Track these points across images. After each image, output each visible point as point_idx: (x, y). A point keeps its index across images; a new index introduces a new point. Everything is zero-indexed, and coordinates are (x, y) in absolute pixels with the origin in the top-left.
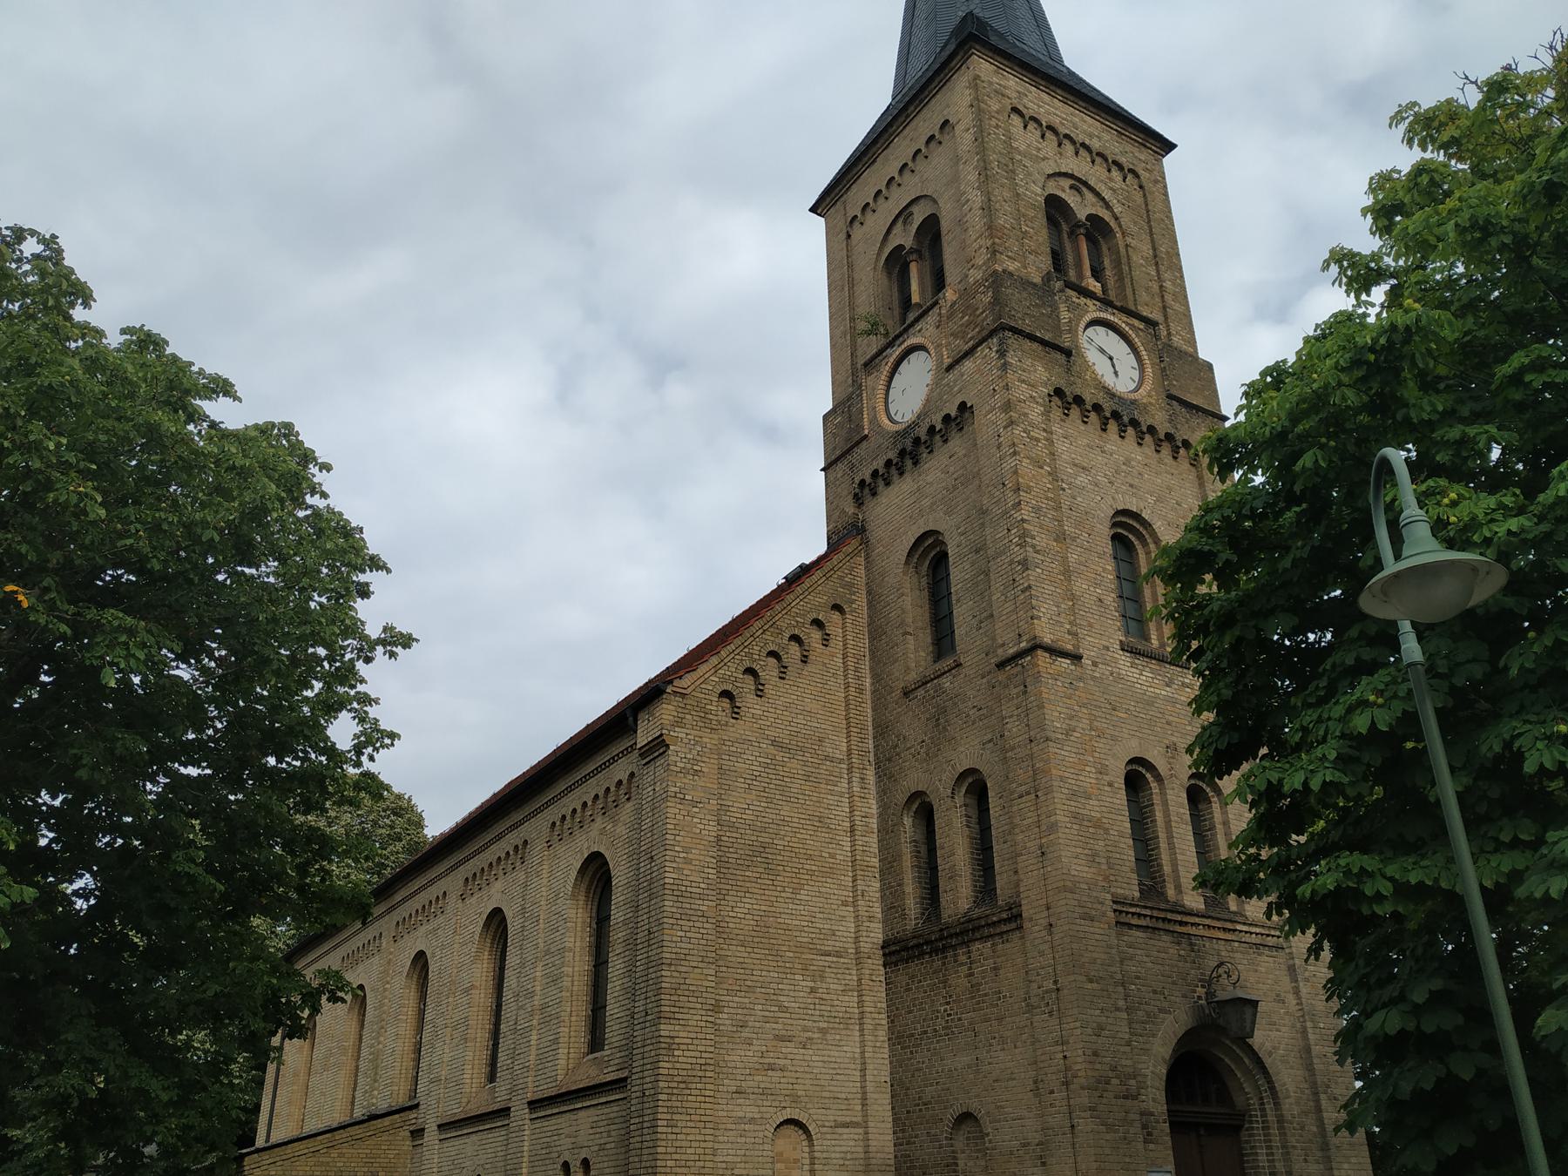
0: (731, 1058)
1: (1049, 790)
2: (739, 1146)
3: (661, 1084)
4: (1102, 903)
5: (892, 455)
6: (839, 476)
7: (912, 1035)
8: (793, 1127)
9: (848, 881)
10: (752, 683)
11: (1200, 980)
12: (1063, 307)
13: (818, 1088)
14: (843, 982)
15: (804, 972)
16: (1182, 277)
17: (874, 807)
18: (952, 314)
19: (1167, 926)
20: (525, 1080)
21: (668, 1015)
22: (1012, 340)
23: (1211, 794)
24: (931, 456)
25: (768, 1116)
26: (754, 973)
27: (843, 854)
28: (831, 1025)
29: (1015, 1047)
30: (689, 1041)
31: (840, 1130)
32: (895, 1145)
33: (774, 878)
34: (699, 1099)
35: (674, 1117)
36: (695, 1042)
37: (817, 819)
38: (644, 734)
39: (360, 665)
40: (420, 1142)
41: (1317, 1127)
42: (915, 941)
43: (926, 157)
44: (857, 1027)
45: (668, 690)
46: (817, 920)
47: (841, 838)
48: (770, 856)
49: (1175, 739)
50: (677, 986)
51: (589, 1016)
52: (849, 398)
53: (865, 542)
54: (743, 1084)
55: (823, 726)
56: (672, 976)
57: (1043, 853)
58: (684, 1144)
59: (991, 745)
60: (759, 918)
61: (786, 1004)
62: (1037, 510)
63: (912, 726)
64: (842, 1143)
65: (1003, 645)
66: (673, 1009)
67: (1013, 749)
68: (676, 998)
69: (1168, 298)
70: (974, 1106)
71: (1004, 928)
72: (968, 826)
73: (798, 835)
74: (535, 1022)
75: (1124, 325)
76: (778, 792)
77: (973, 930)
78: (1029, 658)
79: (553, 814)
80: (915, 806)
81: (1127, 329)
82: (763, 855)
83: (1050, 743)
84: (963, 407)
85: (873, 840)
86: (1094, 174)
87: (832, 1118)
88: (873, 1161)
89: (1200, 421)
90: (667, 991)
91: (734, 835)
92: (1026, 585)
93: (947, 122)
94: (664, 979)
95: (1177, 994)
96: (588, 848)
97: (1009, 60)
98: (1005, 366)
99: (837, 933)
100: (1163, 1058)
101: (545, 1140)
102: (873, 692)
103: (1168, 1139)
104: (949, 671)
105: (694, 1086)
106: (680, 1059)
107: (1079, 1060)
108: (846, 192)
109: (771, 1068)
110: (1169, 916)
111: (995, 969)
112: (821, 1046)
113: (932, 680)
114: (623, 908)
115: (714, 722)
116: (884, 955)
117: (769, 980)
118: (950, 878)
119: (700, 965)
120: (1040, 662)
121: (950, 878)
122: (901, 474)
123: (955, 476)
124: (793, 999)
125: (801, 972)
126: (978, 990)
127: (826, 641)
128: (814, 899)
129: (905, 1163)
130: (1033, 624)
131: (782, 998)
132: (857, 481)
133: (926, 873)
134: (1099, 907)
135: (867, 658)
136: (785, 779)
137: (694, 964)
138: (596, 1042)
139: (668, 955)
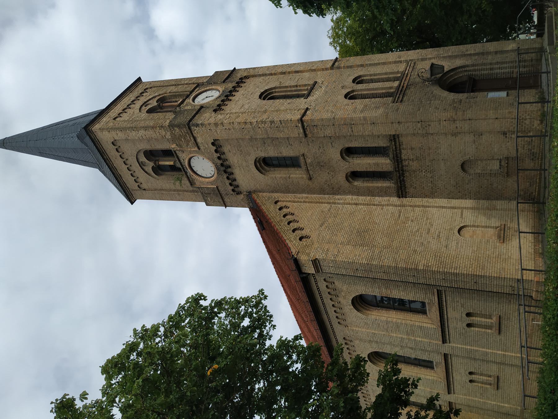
0: (434, 248)
1: (352, 119)
2: (466, 248)
3: (441, 270)
4: (393, 106)
5: (225, 176)
6: (229, 201)
7: (432, 187)
8: (461, 232)
9: (374, 207)
10: (298, 231)
11: (423, 83)
12: (186, 108)
13: (448, 222)
14: (410, 211)
15: (405, 223)
16: (184, 79)
17: (349, 197)
18: (180, 146)
19: (403, 91)
20: (434, 344)
21: (416, 266)
22: (194, 121)
23: (360, 79)
24: (228, 160)
25: (456, 238)
26: (403, 238)
27: (365, 208)
28: (426, 216)
29: (440, 143)
30: (426, 260)
31: (464, 217)
32: (470, 199)
33: (370, 230)
34: (448, 258)
35: (453, 267)
36: (426, 258)
37: (350, 215)
38: (310, 269)
39: (268, 339)
40: (454, 404)
41: (476, 56)
42: (399, 183)
43: (123, 153)
44: (427, 208)
45: (296, 257)
46: (387, 218)
47: (359, 208)
48: (362, 230)
49: (340, 86)
50: (405, 263)
51: (413, 314)
52: (202, 193)
53: (255, 192)
54: (444, 245)
55: (318, 210)
56: (401, 264)
57: (373, 123)
58: (464, 264)
59: (333, 143)
60: (384, 236)
61: (416, 230)
62: (254, 117)
63: (322, 177)
64: (468, 216)
65: (299, 134)
66: (414, 264)
67: (335, 133)
68: (410, 263)
69: (190, 82)
70: (459, 163)
71: (398, 144)
72: (361, 157)
73: (356, 221)
74: (413, 338)
75: (196, 93)
76: (339, 226)
77: (397, 157)
78: (305, 123)
79: (335, 322)
80: (351, 180)
81: (198, 92)
82: (361, 232)
83: (336, 117)
84: (213, 144)
85: (360, 198)
86: (143, 100)
87: (459, 219)
88: (476, 206)
89: (234, 75)
90: (407, 266)
91: (352, 241)
92: (279, 122)
93: (113, 143)
94: (402, 266)
95: (427, 89)
96: (350, 305)
97: (96, 119)
98: (202, 124)
99: (393, 212)
100: (448, 93)
101: (458, 336)
102: (308, 194)
103: (476, 93)
104: (305, 159)
105: (443, 260)
106: (432, 263)
107: (446, 114)
108: (129, 189)
109: (439, 236)
110: (400, 90)
111: (411, 149)
112: (433, 220)
113: (307, 167)
114: (374, 289)
115: (310, 243)
116: (402, 197)
117: (406, 234)
118: (378, 166)
119: (398, 254)
120: (307, 119)
121: (378, 166)
122: (233, 174)
123: (237, 150)
124: (415, 227)
125: (405, 224)
126: (419, 157)
127: (287, 207)
128: (379, 218)
129: (477, 195)
130: (293, 120)
131: (414, 231)
132: (232, 193)
133: (375, 179)
134: (394, 107)
135: (296, 195)
136: (335, 223)
137: (398, 256)
138: (422, 310)
139: (393, 265)
